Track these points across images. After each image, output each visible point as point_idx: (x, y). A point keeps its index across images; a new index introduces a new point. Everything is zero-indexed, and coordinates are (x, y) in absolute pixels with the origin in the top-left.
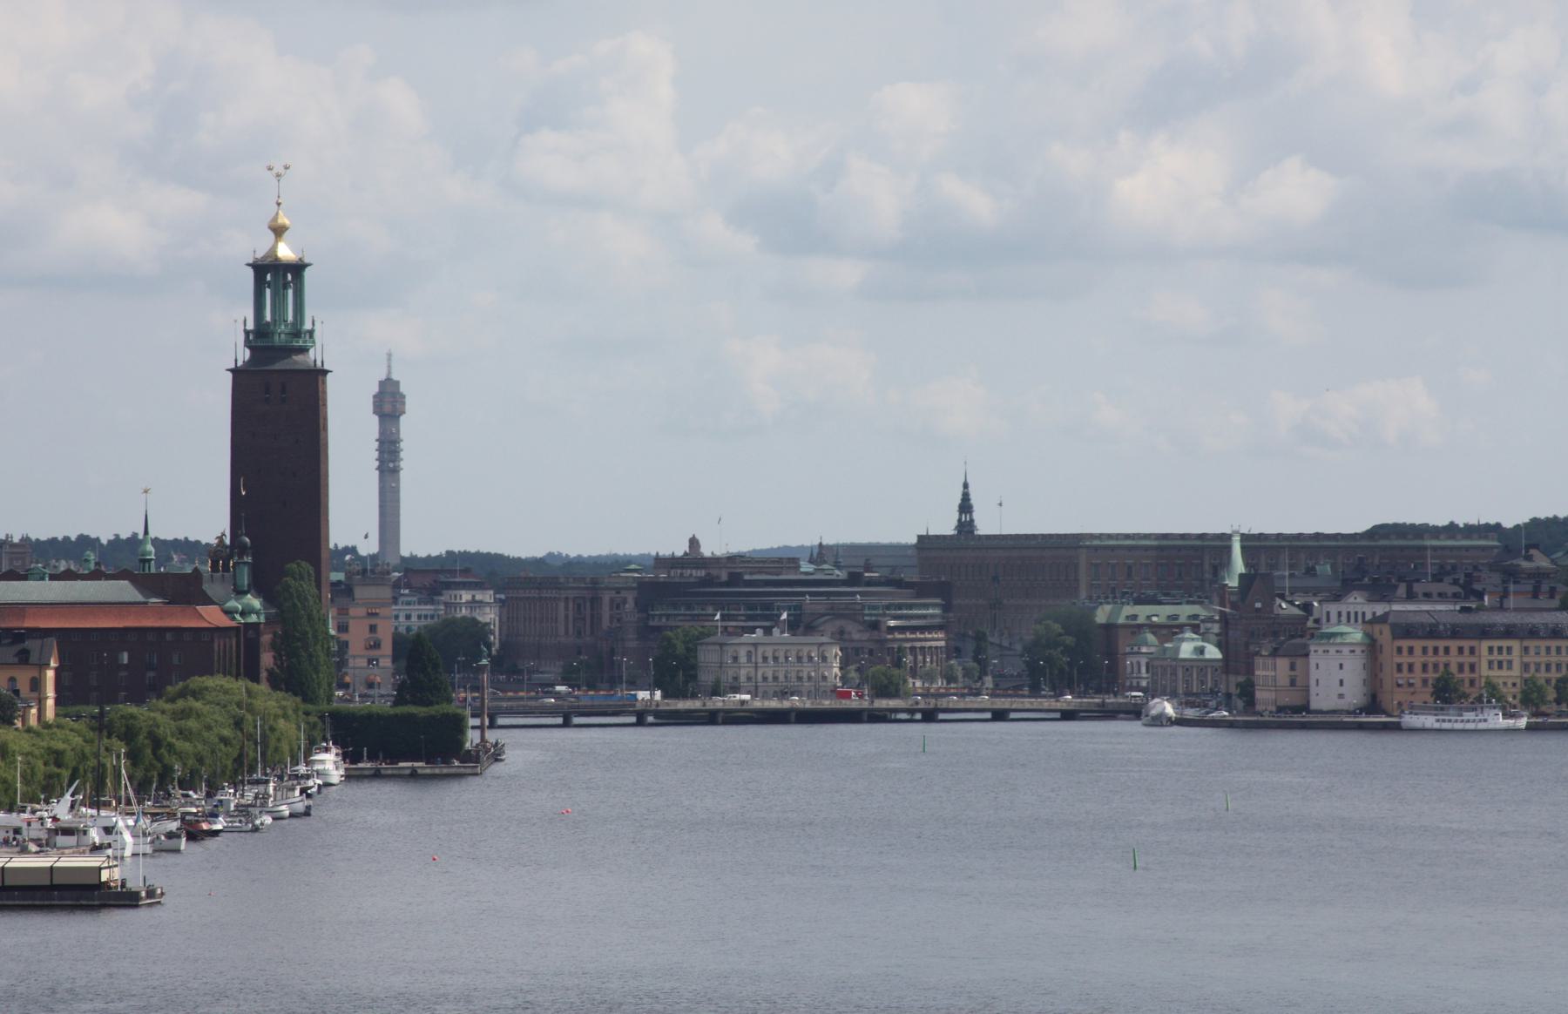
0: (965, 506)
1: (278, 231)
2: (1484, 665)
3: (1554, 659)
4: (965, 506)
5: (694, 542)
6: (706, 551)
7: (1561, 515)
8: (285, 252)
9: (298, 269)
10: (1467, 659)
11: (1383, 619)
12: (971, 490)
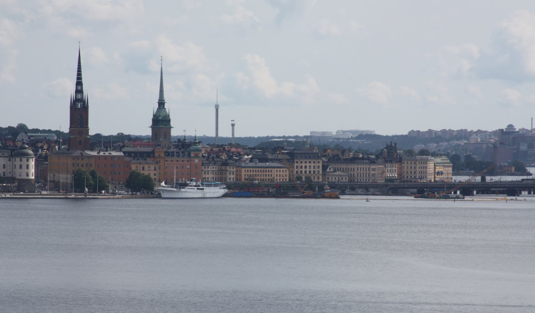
2: (297, 165)
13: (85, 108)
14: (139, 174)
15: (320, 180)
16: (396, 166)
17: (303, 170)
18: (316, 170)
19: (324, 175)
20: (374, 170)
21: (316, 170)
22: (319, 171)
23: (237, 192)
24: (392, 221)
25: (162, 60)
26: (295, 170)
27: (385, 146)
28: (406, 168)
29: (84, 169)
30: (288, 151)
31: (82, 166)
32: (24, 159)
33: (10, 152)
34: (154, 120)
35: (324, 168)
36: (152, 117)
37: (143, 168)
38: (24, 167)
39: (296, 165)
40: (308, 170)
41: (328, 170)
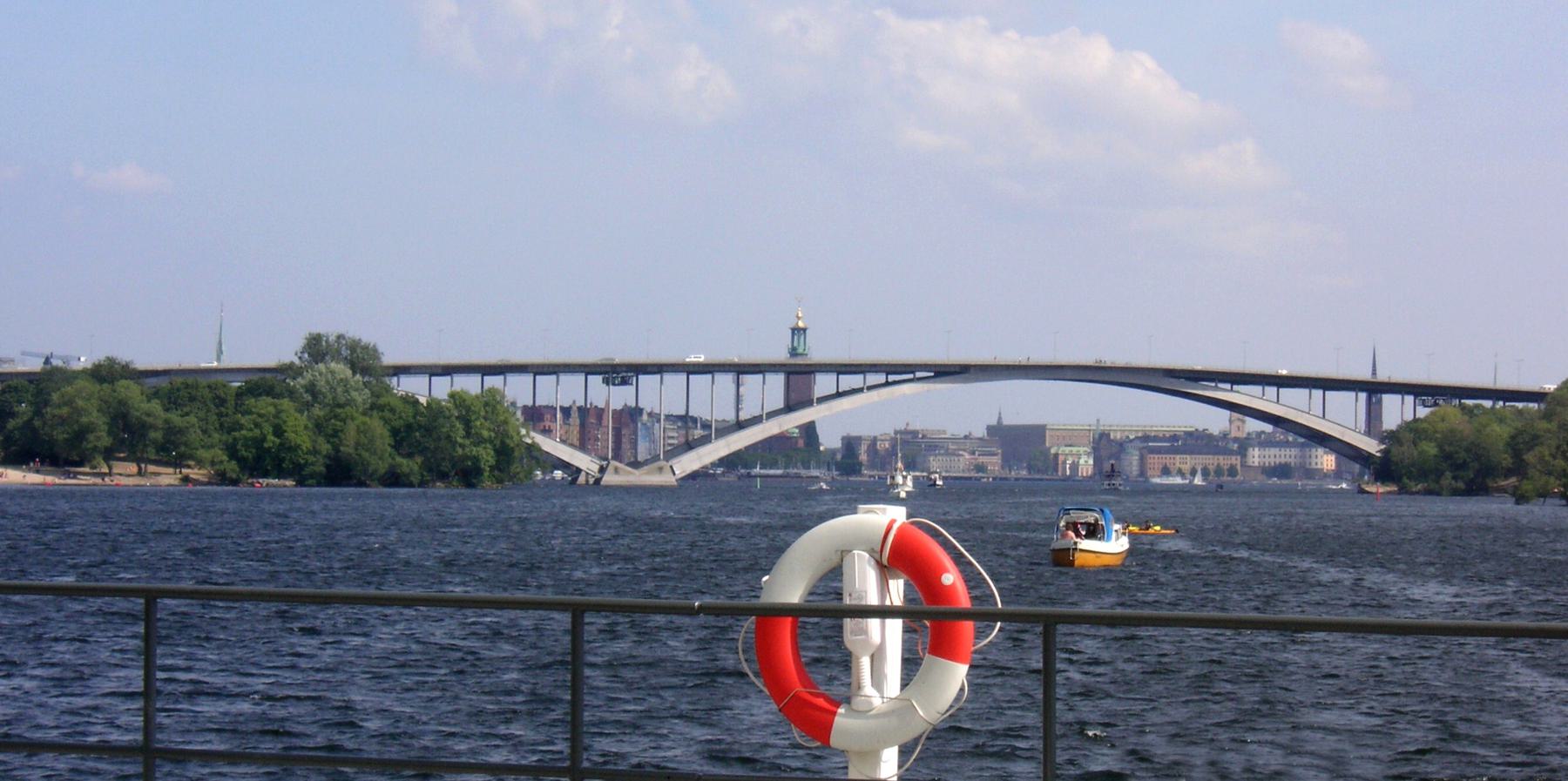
0: (1000, 418)
1: (799, 318)
4: (1000, 418)
6: (1006, 422)
8: (801, 324)
9: (804, 330)
11: (1144, 448)
12: (1002, 416)
38: (1313, 456)
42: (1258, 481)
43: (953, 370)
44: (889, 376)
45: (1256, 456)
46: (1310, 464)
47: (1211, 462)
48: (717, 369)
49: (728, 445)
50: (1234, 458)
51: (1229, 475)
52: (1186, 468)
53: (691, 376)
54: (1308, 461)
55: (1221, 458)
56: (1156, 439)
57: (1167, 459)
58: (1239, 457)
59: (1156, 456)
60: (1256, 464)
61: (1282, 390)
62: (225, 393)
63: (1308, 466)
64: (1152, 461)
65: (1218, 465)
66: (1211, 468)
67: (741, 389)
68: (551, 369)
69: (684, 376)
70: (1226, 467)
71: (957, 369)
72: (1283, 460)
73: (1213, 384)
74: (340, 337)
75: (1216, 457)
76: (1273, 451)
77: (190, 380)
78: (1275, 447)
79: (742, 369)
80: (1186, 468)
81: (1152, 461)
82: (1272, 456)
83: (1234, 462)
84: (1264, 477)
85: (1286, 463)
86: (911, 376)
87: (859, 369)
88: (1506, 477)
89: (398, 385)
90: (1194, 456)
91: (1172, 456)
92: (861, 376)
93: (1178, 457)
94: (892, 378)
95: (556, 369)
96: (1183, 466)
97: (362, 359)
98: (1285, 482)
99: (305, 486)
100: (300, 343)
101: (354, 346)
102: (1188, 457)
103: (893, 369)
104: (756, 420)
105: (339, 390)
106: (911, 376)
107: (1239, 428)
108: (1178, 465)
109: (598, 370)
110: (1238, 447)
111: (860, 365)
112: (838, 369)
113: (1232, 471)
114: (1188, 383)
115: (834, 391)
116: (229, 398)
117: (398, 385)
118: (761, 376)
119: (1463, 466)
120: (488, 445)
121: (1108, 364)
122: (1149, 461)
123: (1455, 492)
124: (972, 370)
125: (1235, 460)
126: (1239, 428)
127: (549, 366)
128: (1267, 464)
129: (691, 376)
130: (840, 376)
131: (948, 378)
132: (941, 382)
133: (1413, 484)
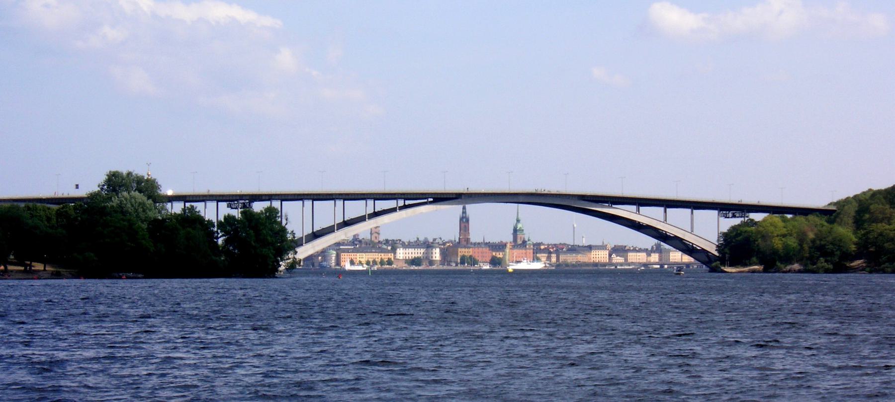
3: (373, 257)
5: (418, 239)
7: (882, 184)
10: (355, 257)
13: (468, 221)
14: (496, 257)
15: (608, 261)
16: (29, 263)
17: (597, 256)
18: (605, 256)
19: (609, 259)
20: (639, 256)
21: (605, 256)
22: (606, 257)
23: (486, 271)
24: (172, 307)
25: (141, 190)
26: (592, 256)
27: (654, 244)
28: (664, 256)
29: (466, 254)
30: (341, 247)
31: (465, 252)
32: (430, 249)
33: (780, 244)
34: (514, 230)
35: (610, 255)
36: (513, 228)
37: (499, 254)
38: (434, 253)
39: (592, 253)
40: (600, 256)
41: (612, 256)
42: (405, 267)
43: (451, 197)
44: (406, 201)
45: (401, 253)
46: (432, 257)
47: (377, 257)
48: (306, 197)
49: (313, 247)
50: (390, 254)
51: (388, 264)
52: (364, 260)
53: (283, 202)
54: (430, 255)
55: (383, 254)
56: (343, 244)
57: (353, 256)
58: (392, 254)
59: (346, 254)
60: (401, 258)
61: (695, 211)
62: (50, 214)
63: (431, 259)
64: (344, 257)
65: (381, 258)
66: (371, 260)
67: (206, 210)
68: (201, 199)
69: (403, 200)
70: (385, 260)
71: (454, 196)
72: (416, 256)
73: (607, 205)
74: (129, 174)
75: (380, 254)
76: (411, 250)
77: (31, 204)
78: (412, 248)
79: (188, 199)
80: (364, 260)
81: (344, 257)
82: (410, 253)
83: (390, 256)
84: (406, 265)
85: (418, 257)
86: (426, 201)
87: (393, 197)
88: (884, 264)
89: (172, 208)
90: (367, 254)
91: (355, 254)
92: (395, 201)
93: (358, 254)
94: (408, 202)
95: (205, 198)
96: (361, 260)
97: (148, 187)
98: (58, 270)
99: (770, 272)
100: (102, 178)
101: (139, 180)
102: (364, 254)
103: (221, 198)
104: (329, 230)
105: (141, 210)
106: (426, 201)
107: (376, 238)
108: (358, 259)
109: (224, 198)
110: (391, 248)
111: (395, 194)
112: (218, 198)
113: (390, 262)
114: (590, 203)
115: (372, 211)
116: (53, 217)
117: (172, 208)
118: (301, 202)
119: (832, 254)
120: (271, 247)
121: (546, 192)
122: (342, 257)
123: (827, 271)
124: (463, 197)
125: (391, 256)
126: (376, 238)
127: (199, 196)
128: (407, 258)
129: (283, 202)
130: (376, 201)
131: (451, 201)
132: (440, 205)
133: (782, 266)
